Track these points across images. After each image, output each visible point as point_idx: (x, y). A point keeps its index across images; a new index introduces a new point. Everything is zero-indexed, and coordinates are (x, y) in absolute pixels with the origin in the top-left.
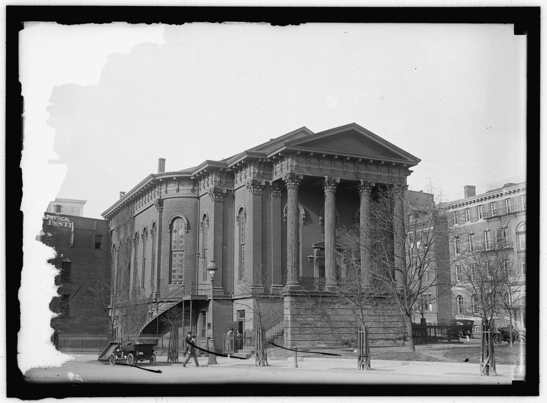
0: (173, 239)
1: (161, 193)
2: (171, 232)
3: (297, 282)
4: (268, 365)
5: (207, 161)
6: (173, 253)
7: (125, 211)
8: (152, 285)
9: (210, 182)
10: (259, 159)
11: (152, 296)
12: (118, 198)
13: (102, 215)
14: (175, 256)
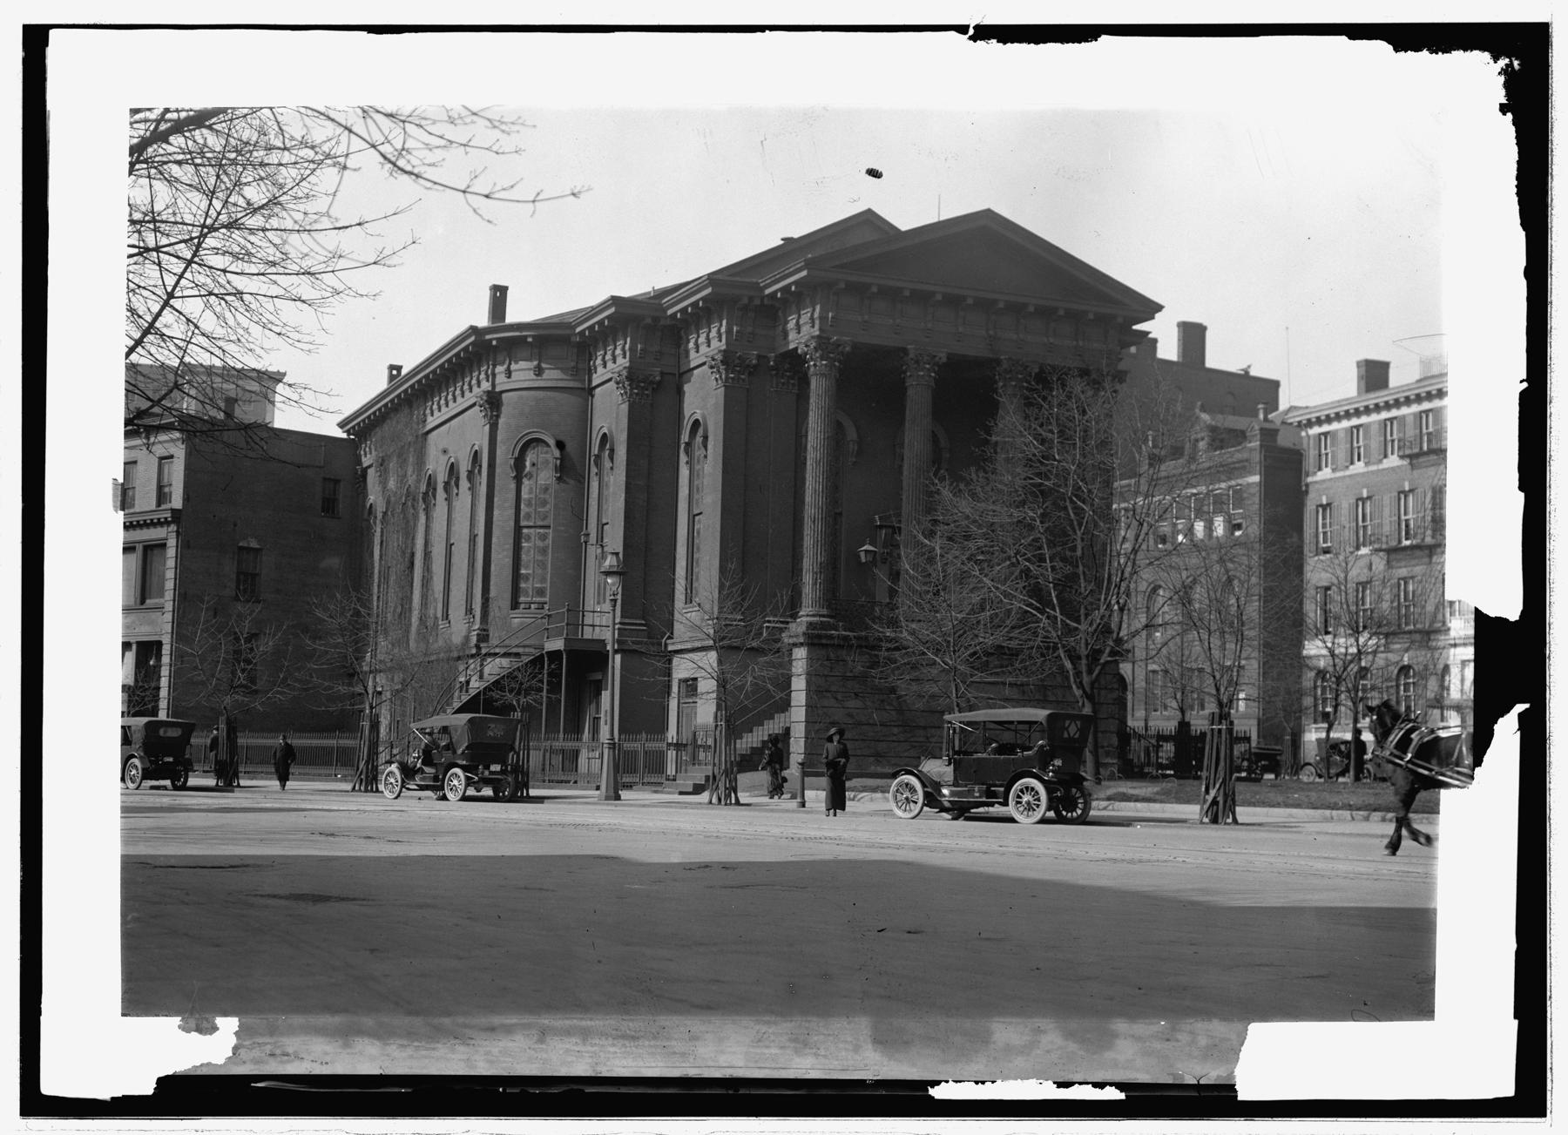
0: (525, 495)
1: (494, 375)
2: (518, 480)
3: (825, 612)
4: (738, 803)
5: (613, 298)
6: (525, 531)
7: (402, 416)
8: (469, 611)
9: (618, 351)
10: (740, 294)
11: (467, 638)
12: (382, 384)
13: (341, 425)
14: (528, 538)
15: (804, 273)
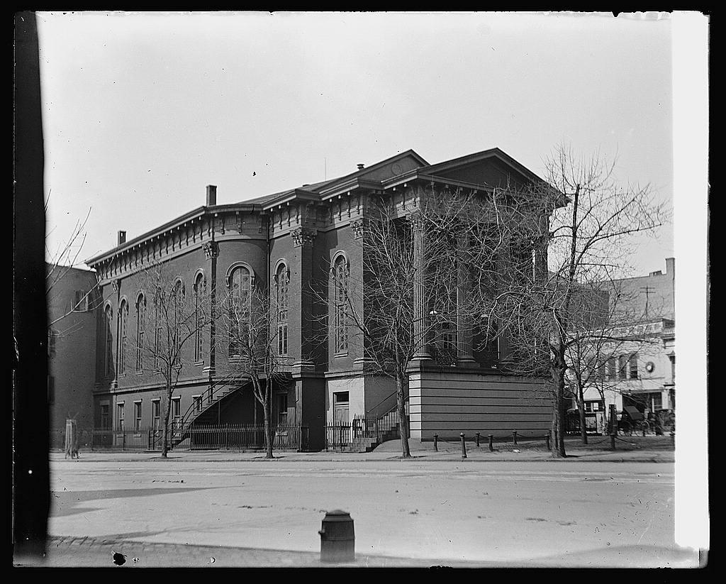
10: (372, 188)
15: (295, 197)
